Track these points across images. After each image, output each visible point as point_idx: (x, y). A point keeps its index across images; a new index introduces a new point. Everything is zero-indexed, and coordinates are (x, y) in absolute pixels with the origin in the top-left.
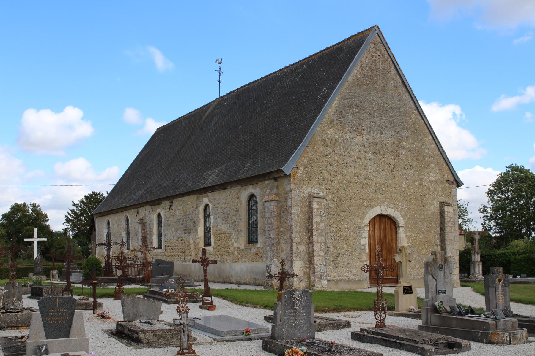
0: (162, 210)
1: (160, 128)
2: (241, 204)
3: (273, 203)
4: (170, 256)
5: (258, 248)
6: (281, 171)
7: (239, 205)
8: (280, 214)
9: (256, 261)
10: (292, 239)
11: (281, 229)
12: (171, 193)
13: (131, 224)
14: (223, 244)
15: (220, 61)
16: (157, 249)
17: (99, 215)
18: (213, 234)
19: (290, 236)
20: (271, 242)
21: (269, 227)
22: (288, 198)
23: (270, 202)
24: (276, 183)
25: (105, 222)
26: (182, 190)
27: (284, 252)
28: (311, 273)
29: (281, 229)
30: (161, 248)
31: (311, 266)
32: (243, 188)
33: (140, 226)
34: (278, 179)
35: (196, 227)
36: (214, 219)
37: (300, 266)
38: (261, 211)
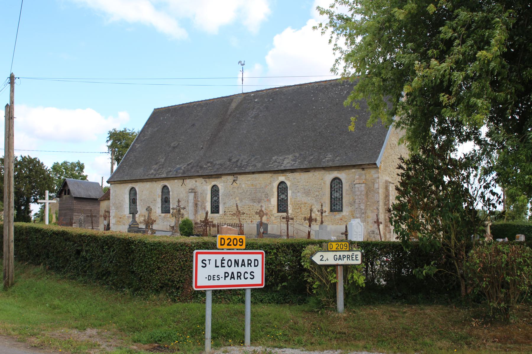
0: (223, 184)
1: (158, 109)
2: (324, 183)
3: (363, 185)
4: (232, 219)
5: (343, 216)
6: (375, 164)
7: (323, 184)
8: (367, 192)
9: (340, 224)
10: (378, 210)
11: (368, 203)
12: (236, 170)
13: (173, 192)
14: (303, 211)
15: (243, 63)
16: (287, 214)
17: (119, 182)
18: (290, 204)
19: (377, 208)
20: (361, 211)
21: (360, 201)
22: (375, 182)
23: (360, 185)
24: (363, 172)
25: (127, 189)
26: (250, 169)
27: (371, 218)
28: (386, 233)
29: (368, 203)
30: (218, 212)
31: (387, 228)
32: (327, 172)
33: (193, 194)
34: (365, 169)
35: (269, 198)
36: (293, 192)
37: (122, 231)
38: (347, 190)
